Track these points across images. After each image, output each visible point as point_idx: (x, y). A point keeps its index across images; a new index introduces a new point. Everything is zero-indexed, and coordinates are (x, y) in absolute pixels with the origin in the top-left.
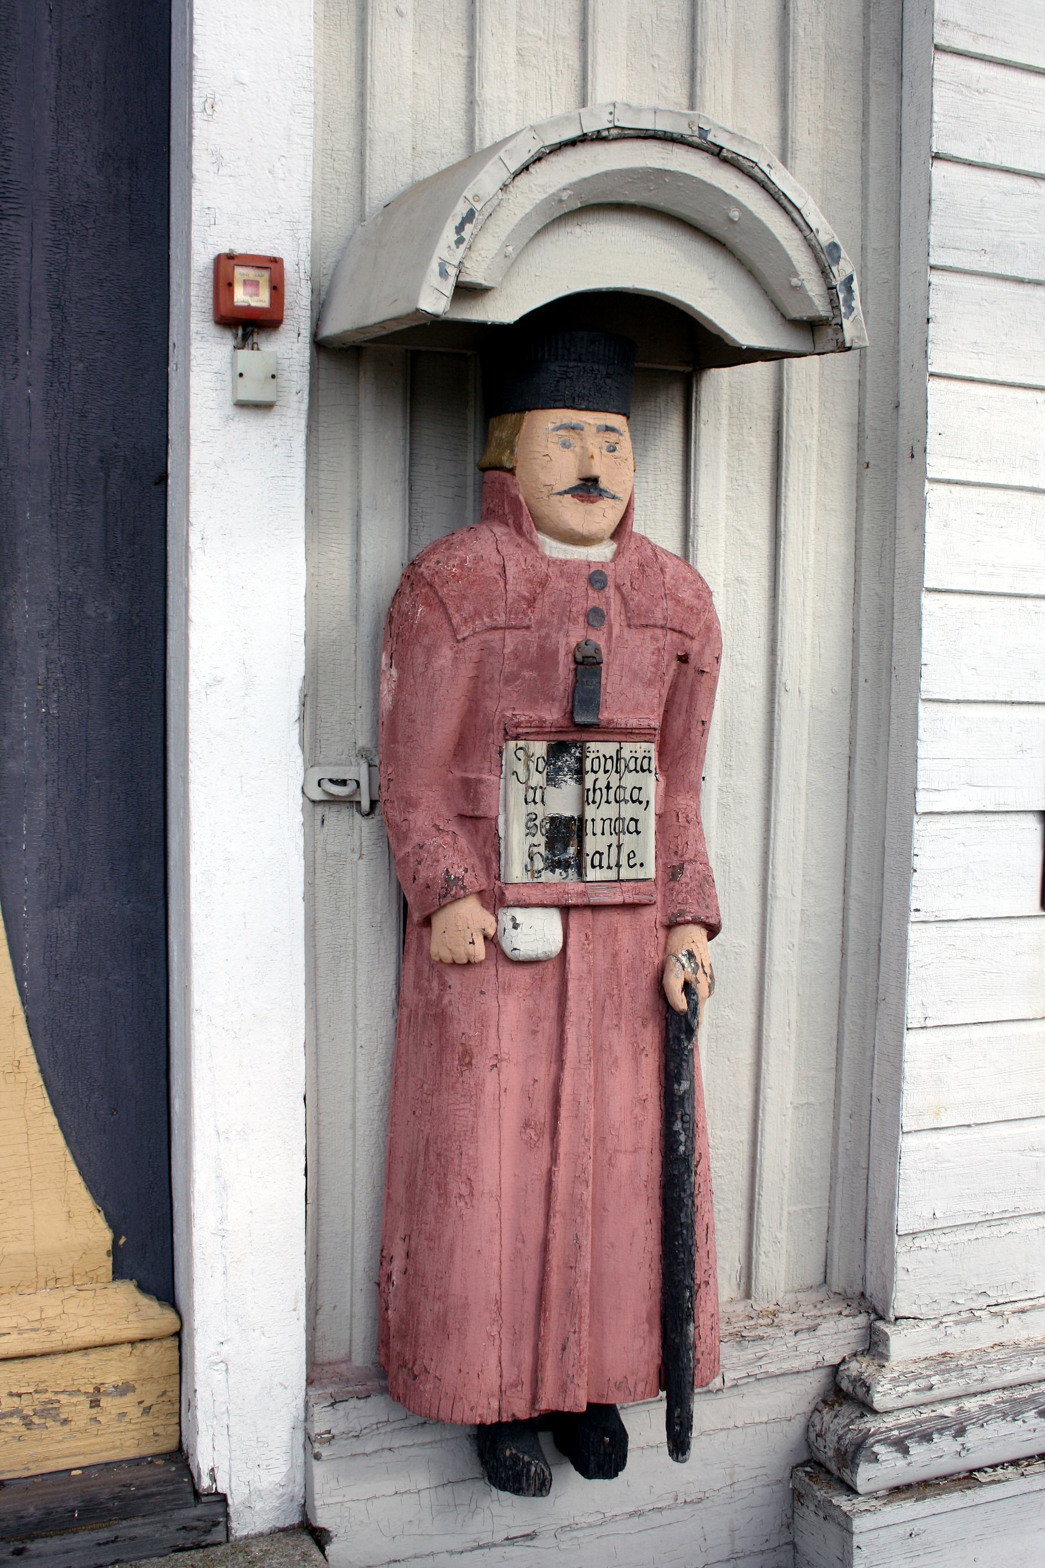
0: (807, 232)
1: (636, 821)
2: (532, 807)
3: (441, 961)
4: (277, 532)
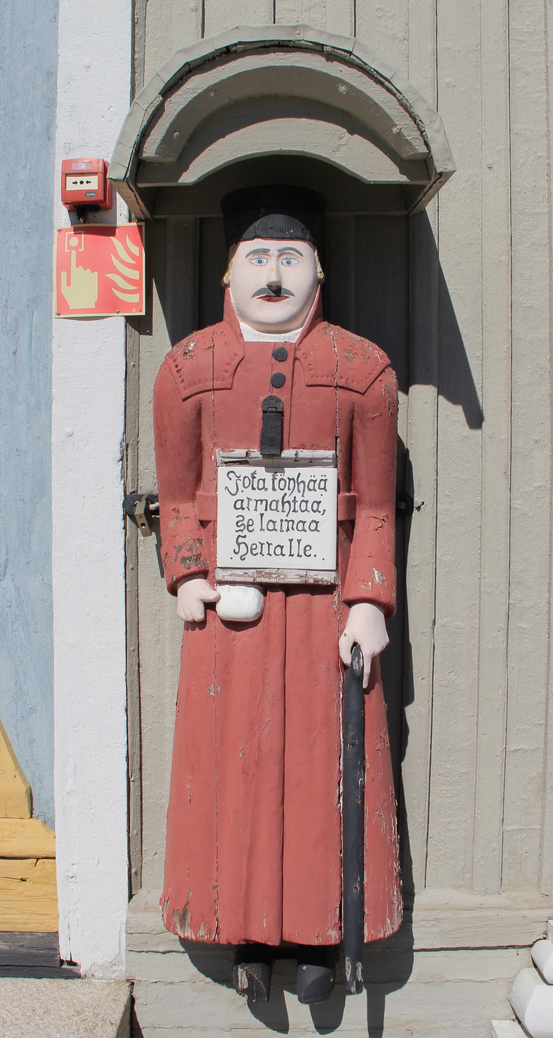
0: (398, 95)
1: (317, 523)
2: (240, 512)
3: (122, 459)
4: (106, 340)
